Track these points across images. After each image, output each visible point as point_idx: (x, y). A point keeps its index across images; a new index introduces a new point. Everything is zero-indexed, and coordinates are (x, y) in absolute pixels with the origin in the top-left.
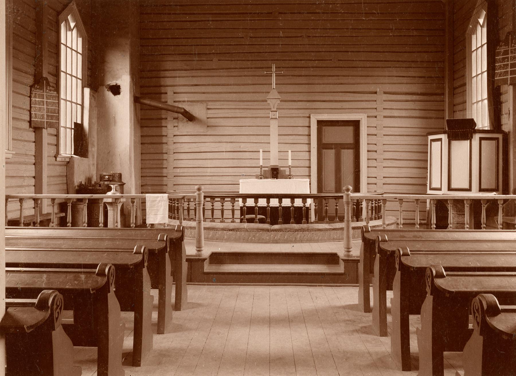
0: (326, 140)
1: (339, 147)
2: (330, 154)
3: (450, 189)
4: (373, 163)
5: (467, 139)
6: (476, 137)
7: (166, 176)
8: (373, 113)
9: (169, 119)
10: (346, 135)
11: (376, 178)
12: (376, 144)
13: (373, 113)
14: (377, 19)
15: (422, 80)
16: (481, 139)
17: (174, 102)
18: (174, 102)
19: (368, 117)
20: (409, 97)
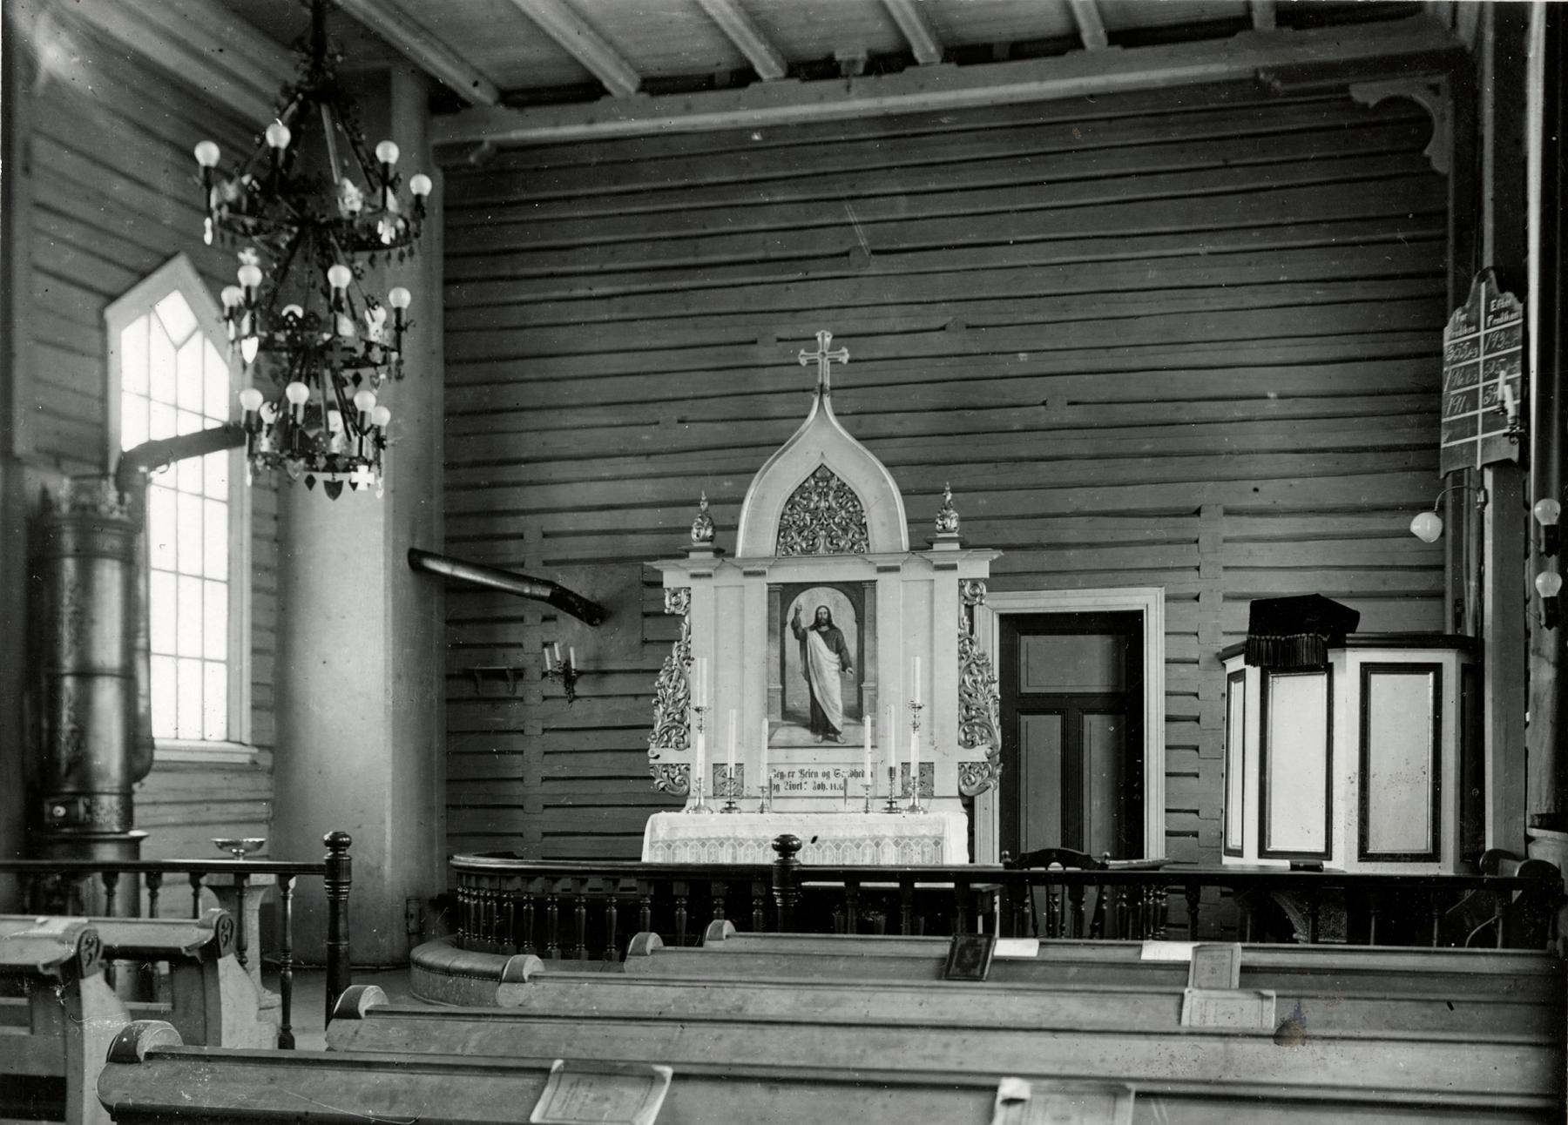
0: (1033, 682)
1: (1068, 707)
2: (1044, 732)
3: (1263, 853)
4: (1187, 761)
5: (1311, 669)
6: (1349, 664)
7: (521, 807)
8: (1190, 583)
9: (529, 620)
10: (1085, 668)
11: (1196, 812)
12: (1196, 695)
13: (1190, 583)
14: (1409, 234)
15: (1387, 460)
16: (1367, 670)
17: (546, 563)
18: (546, 563)
19: (1168, 599)
20: (1315, 525)
